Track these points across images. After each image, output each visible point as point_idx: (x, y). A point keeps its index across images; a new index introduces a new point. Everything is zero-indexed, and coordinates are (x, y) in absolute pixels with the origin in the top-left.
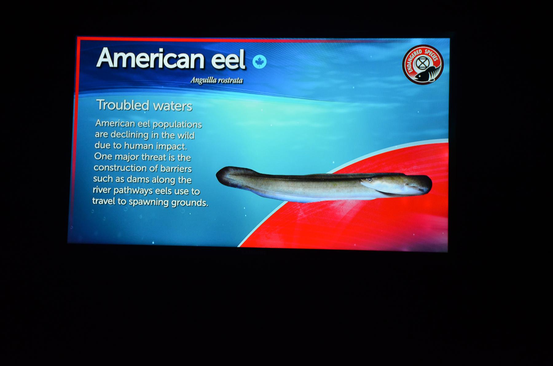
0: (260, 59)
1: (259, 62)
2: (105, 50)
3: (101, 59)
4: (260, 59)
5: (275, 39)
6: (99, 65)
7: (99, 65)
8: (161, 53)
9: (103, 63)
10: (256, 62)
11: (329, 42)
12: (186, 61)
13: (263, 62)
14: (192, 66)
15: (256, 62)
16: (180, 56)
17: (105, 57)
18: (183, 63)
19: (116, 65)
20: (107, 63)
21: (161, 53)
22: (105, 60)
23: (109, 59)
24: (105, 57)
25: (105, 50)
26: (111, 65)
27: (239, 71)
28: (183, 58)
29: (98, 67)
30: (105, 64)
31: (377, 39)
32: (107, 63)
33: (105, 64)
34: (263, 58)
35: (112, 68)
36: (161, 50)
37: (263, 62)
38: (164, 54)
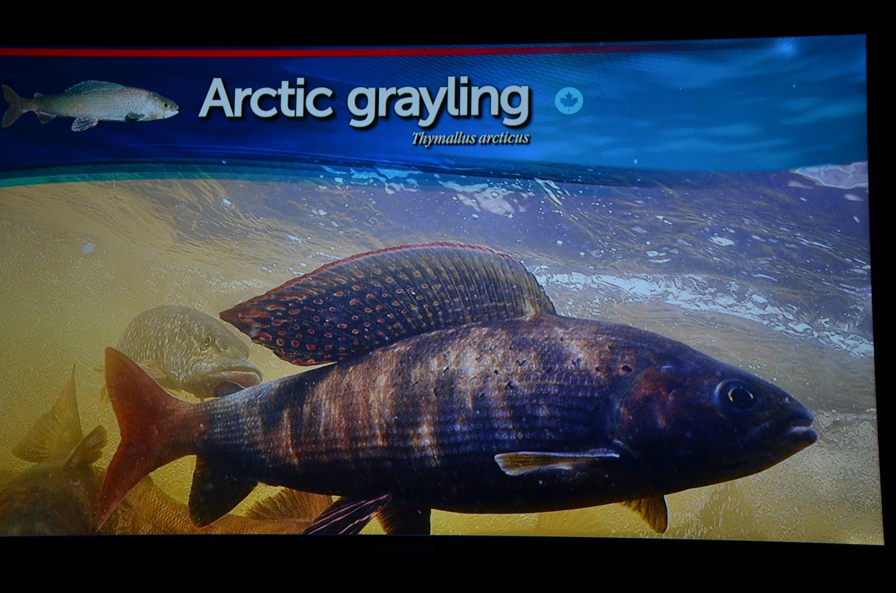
0: (569, 96)
1: (570, 101)
2: (217, 84)
3: (209, 102)
4: (569, 96)
5: (450, 47)
6: (203, 113)
7: (203, 113)
8: (300, 86)
9: (212, 109)
10: (562, 101)
11: (568, 51)
12: (298, 100)
13: (576, 100)
14: (475, 111)
15: (562, 101)
16: (401, 92)
17: (217, 97)
18: (406, 107)
19: (238, 113)
20: (221, 109)
21: (300, 86)
22: (216, 103)
23: (224, 102)
24: (217, 97)
25: (217, 84)
26: (228, 113)
27: (381, 122)
28: (408, 95)
29: (202, 118)
30: (217, 111)
31: (691, 42)
32: (221, 109)
33: (217, 111)
34: (576, 93)
35: (230, 118)
36: (301, 81)
37: (576, 100)
38: (307, 89)
